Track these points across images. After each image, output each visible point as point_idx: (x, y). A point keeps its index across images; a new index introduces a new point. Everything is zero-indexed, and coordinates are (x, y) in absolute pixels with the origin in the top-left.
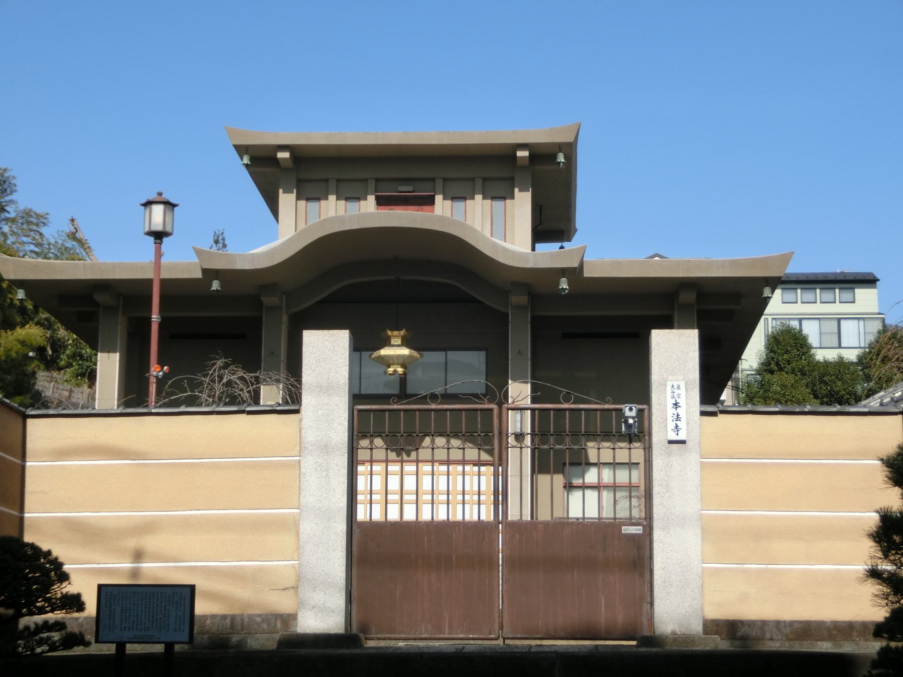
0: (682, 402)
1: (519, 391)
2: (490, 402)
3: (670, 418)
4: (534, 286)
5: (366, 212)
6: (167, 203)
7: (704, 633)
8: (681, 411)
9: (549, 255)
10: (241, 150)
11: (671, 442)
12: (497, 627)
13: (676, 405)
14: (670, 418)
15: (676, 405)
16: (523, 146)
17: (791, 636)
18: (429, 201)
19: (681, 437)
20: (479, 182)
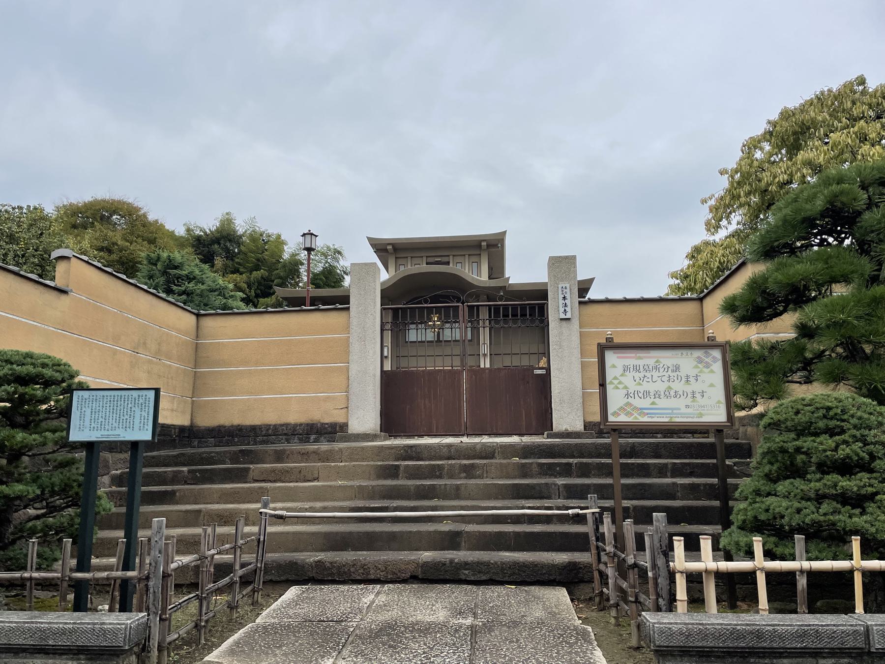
0: (568, 296)
1: (485, 336)
2: (458, 302)
3: (561, 306)
4: (489, 294)
5: (422, 267)
6: (312, 234)
7: (585, 429)
8: (568, 302)
9: (494, 283)
10: (370, 239)
11: (561, 319)
12: (463, 428)
13: (564, 298)
14: (561, 306)
15: (564, 298)
16: (484, 241)
17: (17, 502)
18: (448, 263)
19: (568, 316)
20: (467, 256)
